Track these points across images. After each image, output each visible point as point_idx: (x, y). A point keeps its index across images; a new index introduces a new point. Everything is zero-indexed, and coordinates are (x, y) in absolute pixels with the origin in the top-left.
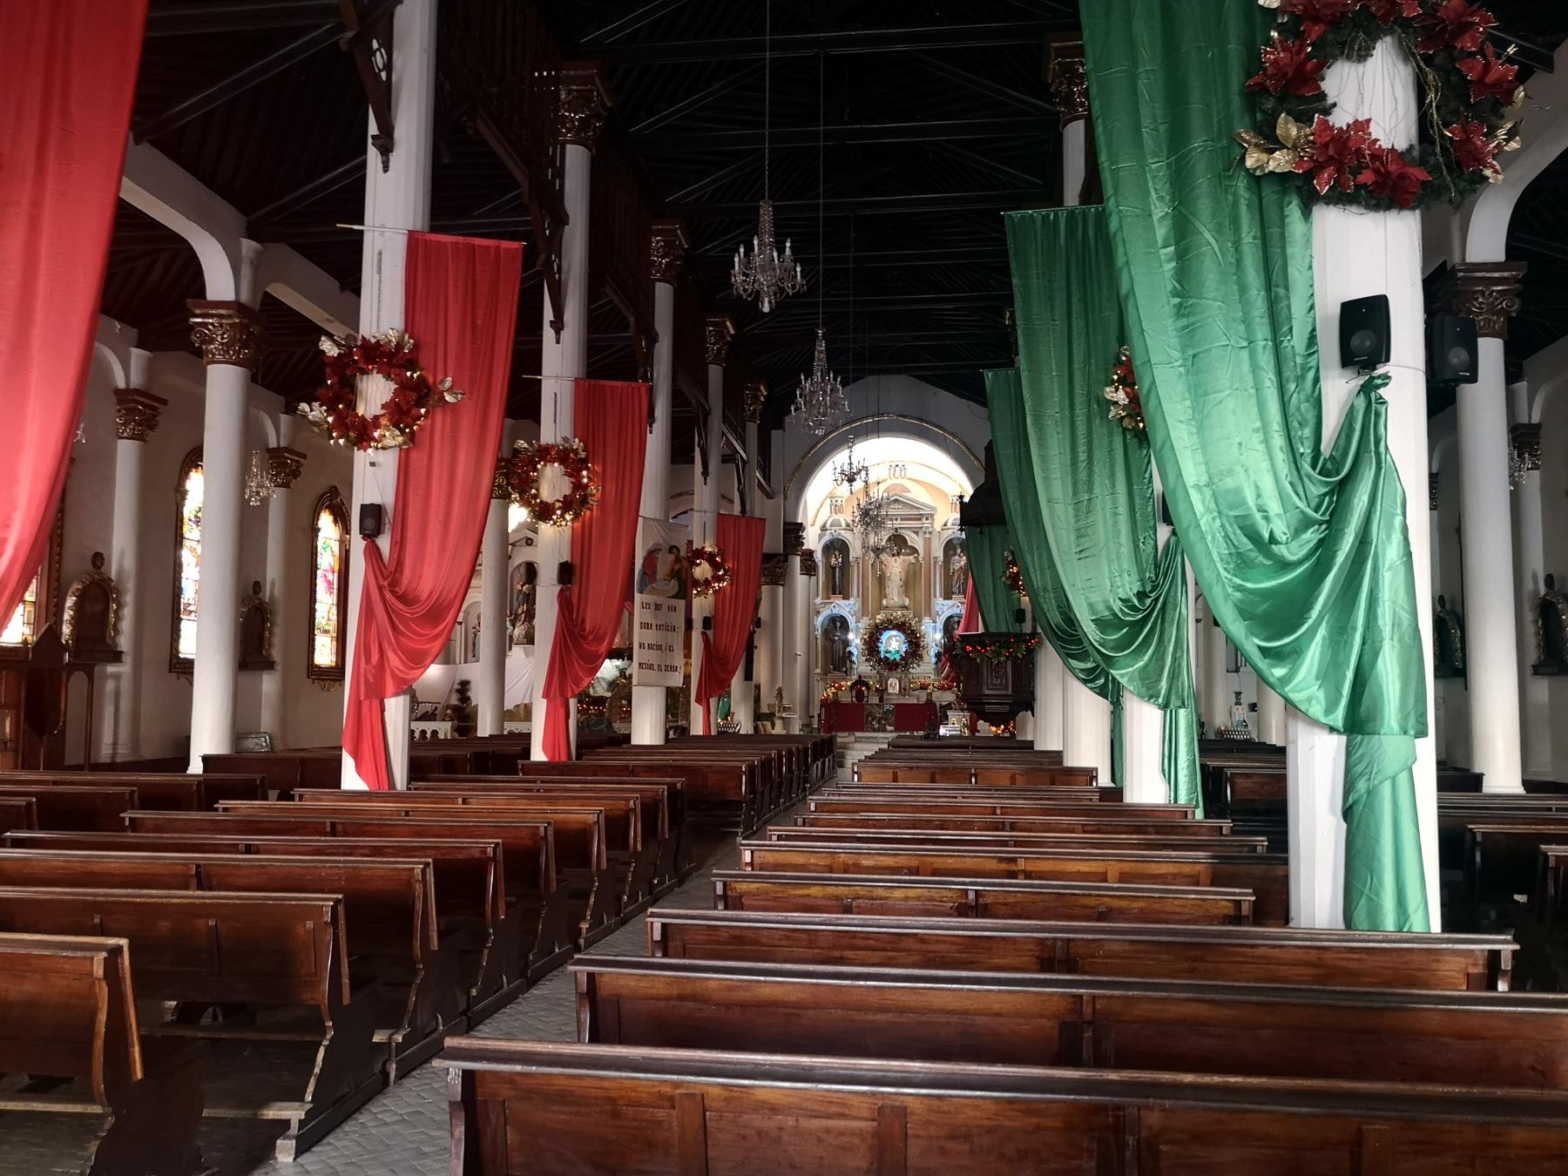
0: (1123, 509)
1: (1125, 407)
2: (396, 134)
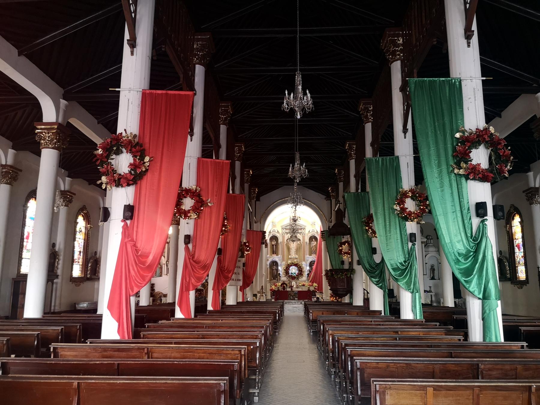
1: (399, 211)
2: (194, 131)
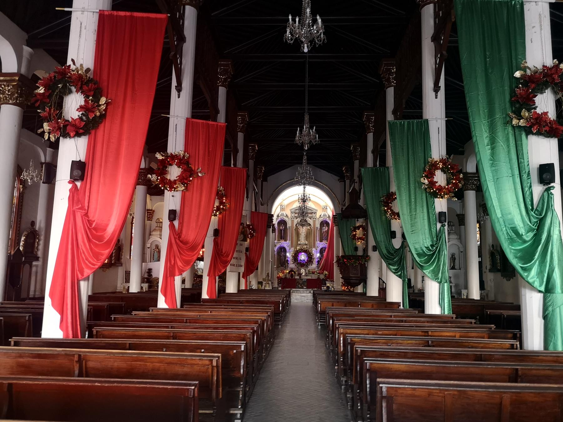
0: (426, 218)
